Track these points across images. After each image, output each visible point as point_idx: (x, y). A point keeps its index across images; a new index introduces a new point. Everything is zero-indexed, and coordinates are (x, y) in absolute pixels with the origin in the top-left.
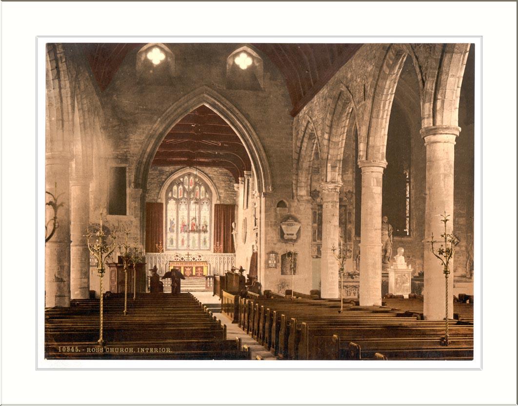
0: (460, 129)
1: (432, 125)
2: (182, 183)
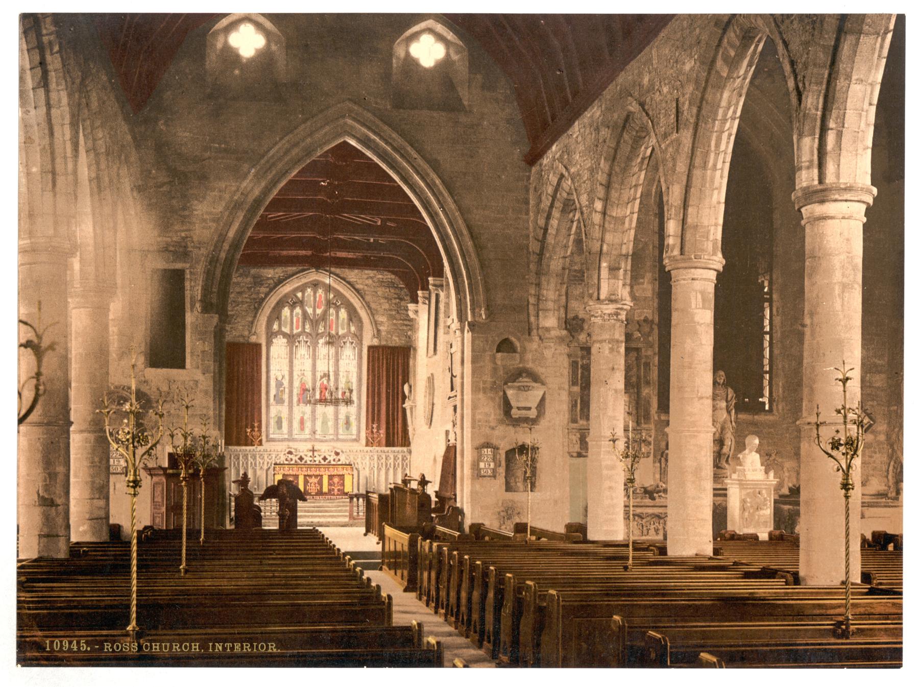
0: (875, 190)
1: (816, 182)
2: (301, 303)
